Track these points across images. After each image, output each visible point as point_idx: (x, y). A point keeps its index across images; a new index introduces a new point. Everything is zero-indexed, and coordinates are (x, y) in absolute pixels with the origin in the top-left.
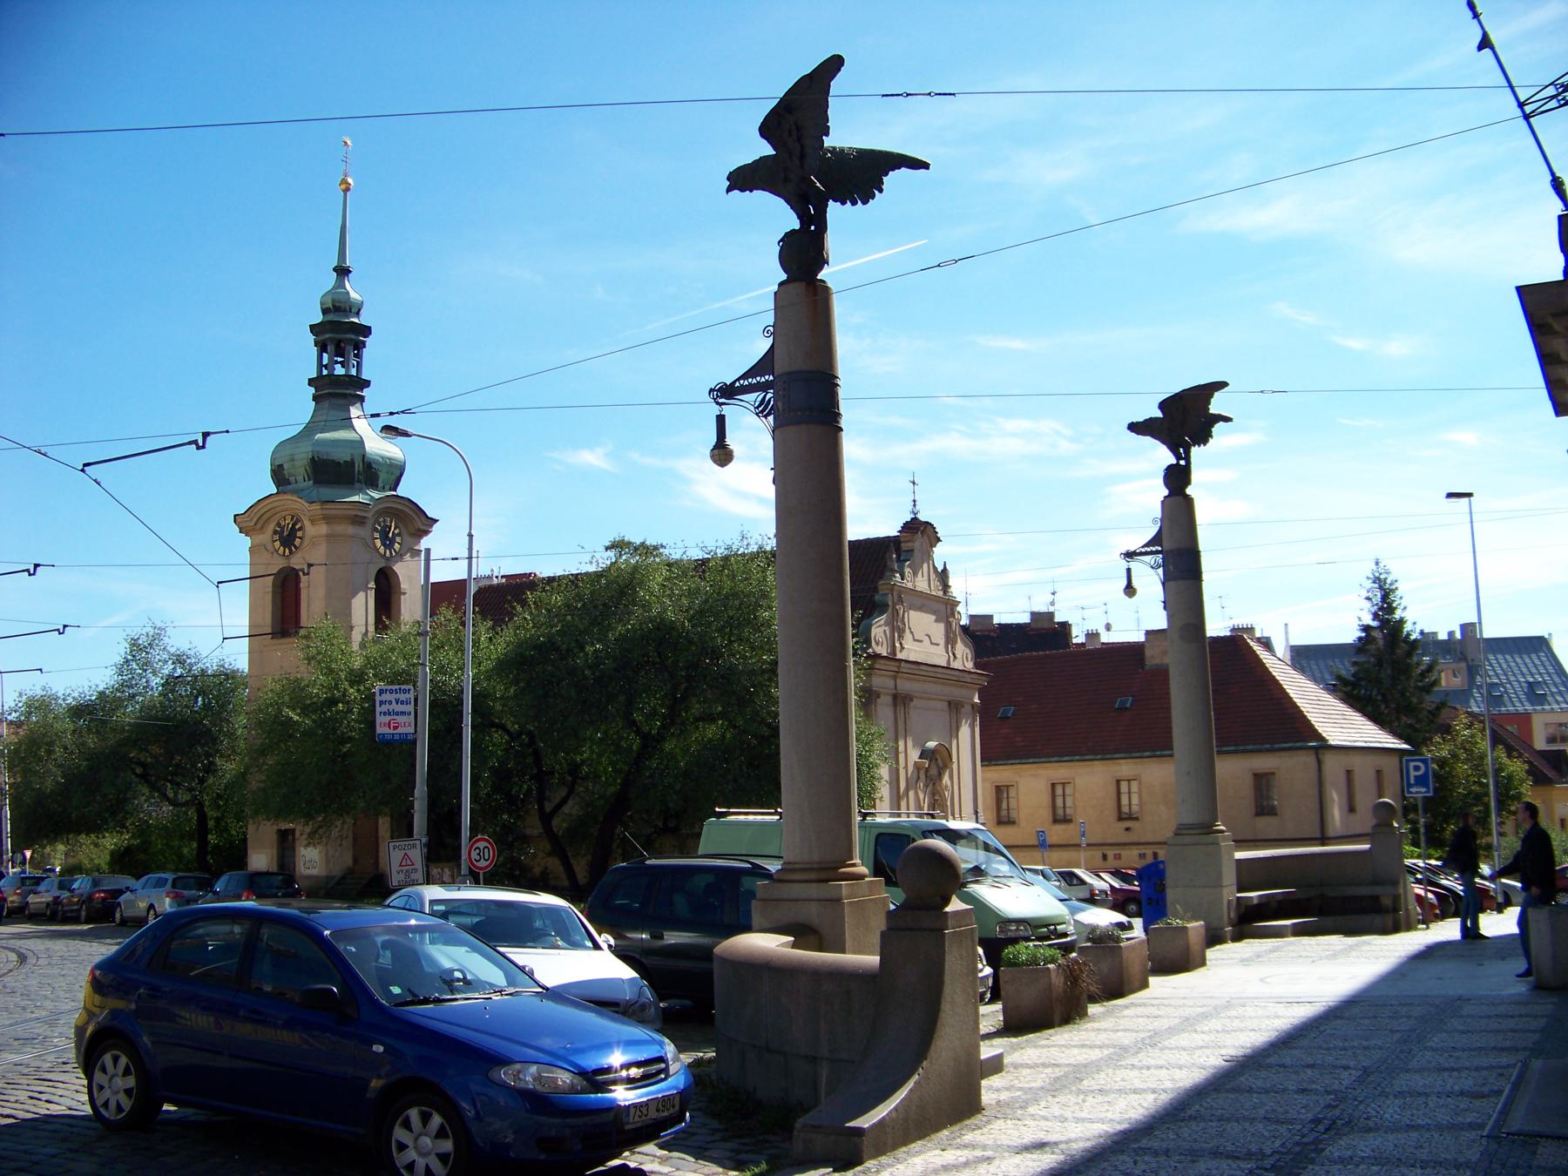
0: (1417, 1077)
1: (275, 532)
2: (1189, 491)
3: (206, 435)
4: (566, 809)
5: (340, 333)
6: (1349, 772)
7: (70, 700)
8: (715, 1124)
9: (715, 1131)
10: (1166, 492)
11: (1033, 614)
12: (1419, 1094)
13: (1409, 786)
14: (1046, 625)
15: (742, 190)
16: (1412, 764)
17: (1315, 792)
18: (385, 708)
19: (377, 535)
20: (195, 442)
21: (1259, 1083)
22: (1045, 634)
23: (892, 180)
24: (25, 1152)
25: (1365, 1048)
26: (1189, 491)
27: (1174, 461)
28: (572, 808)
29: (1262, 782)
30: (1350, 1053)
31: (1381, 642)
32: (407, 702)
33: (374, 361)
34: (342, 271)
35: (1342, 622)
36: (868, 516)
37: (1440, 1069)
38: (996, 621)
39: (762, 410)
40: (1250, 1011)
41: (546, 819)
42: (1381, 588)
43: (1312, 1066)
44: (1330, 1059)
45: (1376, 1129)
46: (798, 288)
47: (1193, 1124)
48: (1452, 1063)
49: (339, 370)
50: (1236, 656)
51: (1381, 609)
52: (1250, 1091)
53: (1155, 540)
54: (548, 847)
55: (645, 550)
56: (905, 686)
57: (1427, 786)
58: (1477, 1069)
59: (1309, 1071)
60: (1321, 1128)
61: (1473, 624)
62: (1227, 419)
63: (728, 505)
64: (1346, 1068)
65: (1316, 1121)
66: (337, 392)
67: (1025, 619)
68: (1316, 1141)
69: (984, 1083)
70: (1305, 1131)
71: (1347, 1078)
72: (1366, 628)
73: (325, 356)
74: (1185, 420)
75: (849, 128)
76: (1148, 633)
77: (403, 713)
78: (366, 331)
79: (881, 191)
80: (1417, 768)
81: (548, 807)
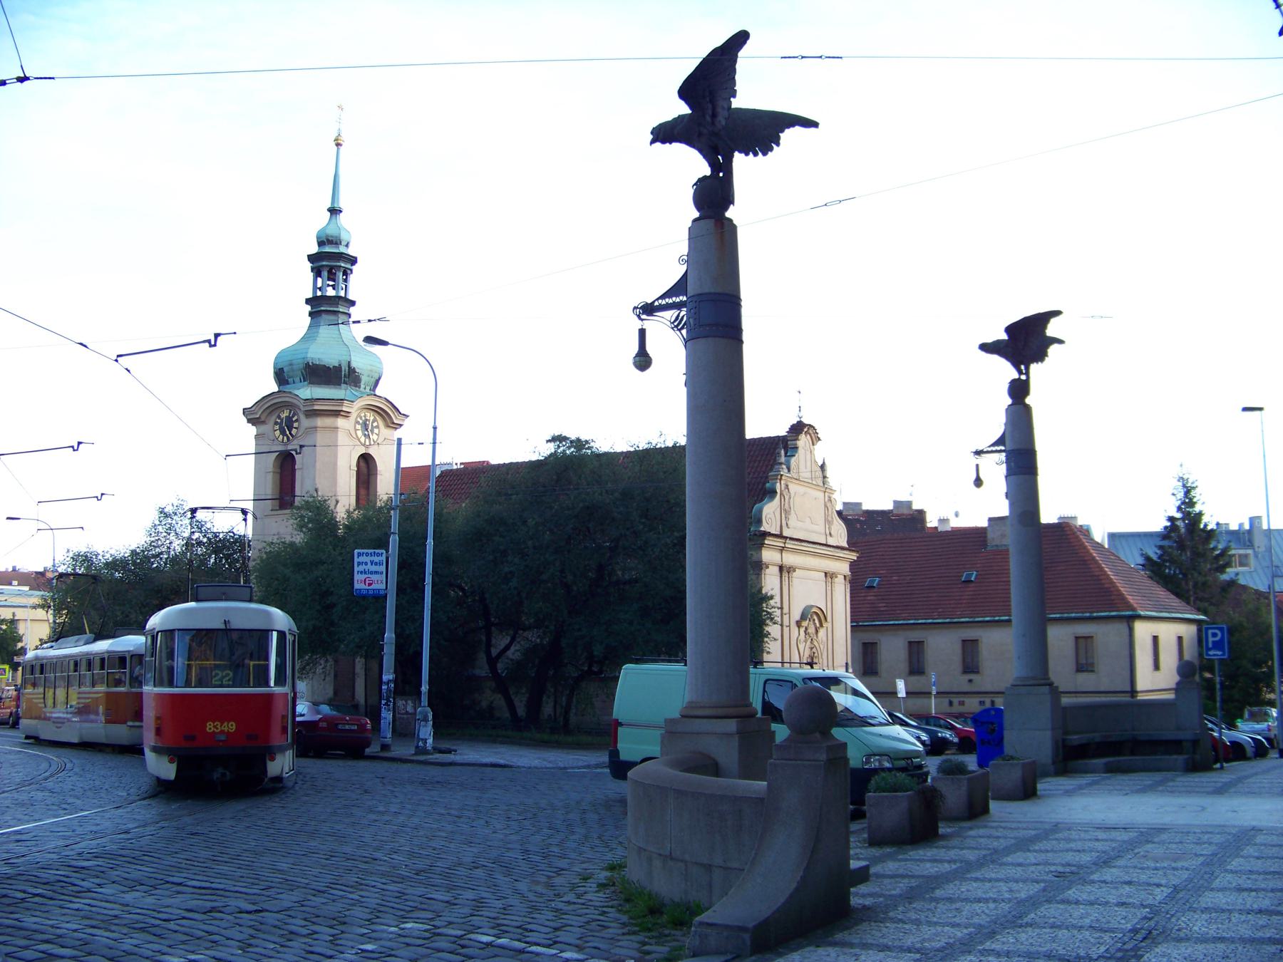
0: (1220, 894)
1: (276, 423)
2: (1028, 401)
3: (217, 336)
4: (509, 653)
5: (330, 261)
6: (1155, 639)
7: (108, 556)
8: (625, 918)
9: (624, 925)
10: (696, 214)
11: (895, 502)
12: (1223, 911)
13: (1208, 649)
14: (905, 511)
15: (663, 142)
16: (1210, 632)
17: (1127, 653)
18: (362, 568)
19: (359, 427)
20: (209, 341)
21: (1085, 896)
22: (906, 521)
23: (790, 136)
24: (52, 927)
25: (1174, 869)
26: (1028, 401)
27: (1015, 375)
28: (514, 653)
29: (1083, 643)
30: (1161, 872)
31: (1183, 530)
32: (380, 564)
33: (358, 285)
34: (334, 211)
35: (1152, 514)
36: (761, 421)
37: (1240, 890)
38: (865, 507)
39: (676, 325)
40: (1074, 835)
41: (492, 662)
42: (1184, 486)
43: (1129, 883)
44: (1143, 878)
45: (1187, 939)
46: (710, 223)
47: (1029, 929)
48: (1249, 884)
49: (330, 292)
50: (1066, 536)
51: (1183, 503)
52: (1077, 902)
53: (1001, 441)
54: (494, 685)
55: (579, 444)
56: (789, 559)
57: (1222, 649)
58: (1272, 890)
59: (1127, 888)
60: (1139, 936)
61: (1259, 518)
62: (1060, 342)
63: (646, 412)
64: (1158, 885)
65: (1135, 931)
66: (326, 308)
67: (888, 506)
68: (1136, 948)
69: (852, 890)
70: (1126, 939)
71: (1160, 894)
72: (1171, 519)
73: (319, 280)
74: (1026, 341)
75: (752, 91)
76: (990, 520)
77: (376, 572)
78: (354, 261)
79: (778, 145)
80: (1214, 635)
81: (494, 652)
